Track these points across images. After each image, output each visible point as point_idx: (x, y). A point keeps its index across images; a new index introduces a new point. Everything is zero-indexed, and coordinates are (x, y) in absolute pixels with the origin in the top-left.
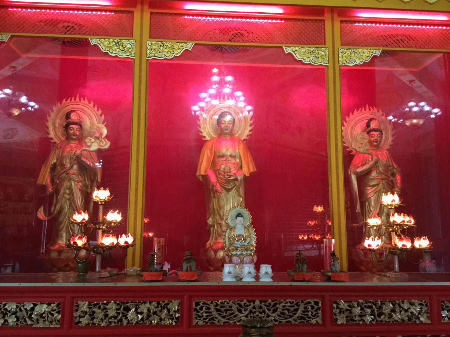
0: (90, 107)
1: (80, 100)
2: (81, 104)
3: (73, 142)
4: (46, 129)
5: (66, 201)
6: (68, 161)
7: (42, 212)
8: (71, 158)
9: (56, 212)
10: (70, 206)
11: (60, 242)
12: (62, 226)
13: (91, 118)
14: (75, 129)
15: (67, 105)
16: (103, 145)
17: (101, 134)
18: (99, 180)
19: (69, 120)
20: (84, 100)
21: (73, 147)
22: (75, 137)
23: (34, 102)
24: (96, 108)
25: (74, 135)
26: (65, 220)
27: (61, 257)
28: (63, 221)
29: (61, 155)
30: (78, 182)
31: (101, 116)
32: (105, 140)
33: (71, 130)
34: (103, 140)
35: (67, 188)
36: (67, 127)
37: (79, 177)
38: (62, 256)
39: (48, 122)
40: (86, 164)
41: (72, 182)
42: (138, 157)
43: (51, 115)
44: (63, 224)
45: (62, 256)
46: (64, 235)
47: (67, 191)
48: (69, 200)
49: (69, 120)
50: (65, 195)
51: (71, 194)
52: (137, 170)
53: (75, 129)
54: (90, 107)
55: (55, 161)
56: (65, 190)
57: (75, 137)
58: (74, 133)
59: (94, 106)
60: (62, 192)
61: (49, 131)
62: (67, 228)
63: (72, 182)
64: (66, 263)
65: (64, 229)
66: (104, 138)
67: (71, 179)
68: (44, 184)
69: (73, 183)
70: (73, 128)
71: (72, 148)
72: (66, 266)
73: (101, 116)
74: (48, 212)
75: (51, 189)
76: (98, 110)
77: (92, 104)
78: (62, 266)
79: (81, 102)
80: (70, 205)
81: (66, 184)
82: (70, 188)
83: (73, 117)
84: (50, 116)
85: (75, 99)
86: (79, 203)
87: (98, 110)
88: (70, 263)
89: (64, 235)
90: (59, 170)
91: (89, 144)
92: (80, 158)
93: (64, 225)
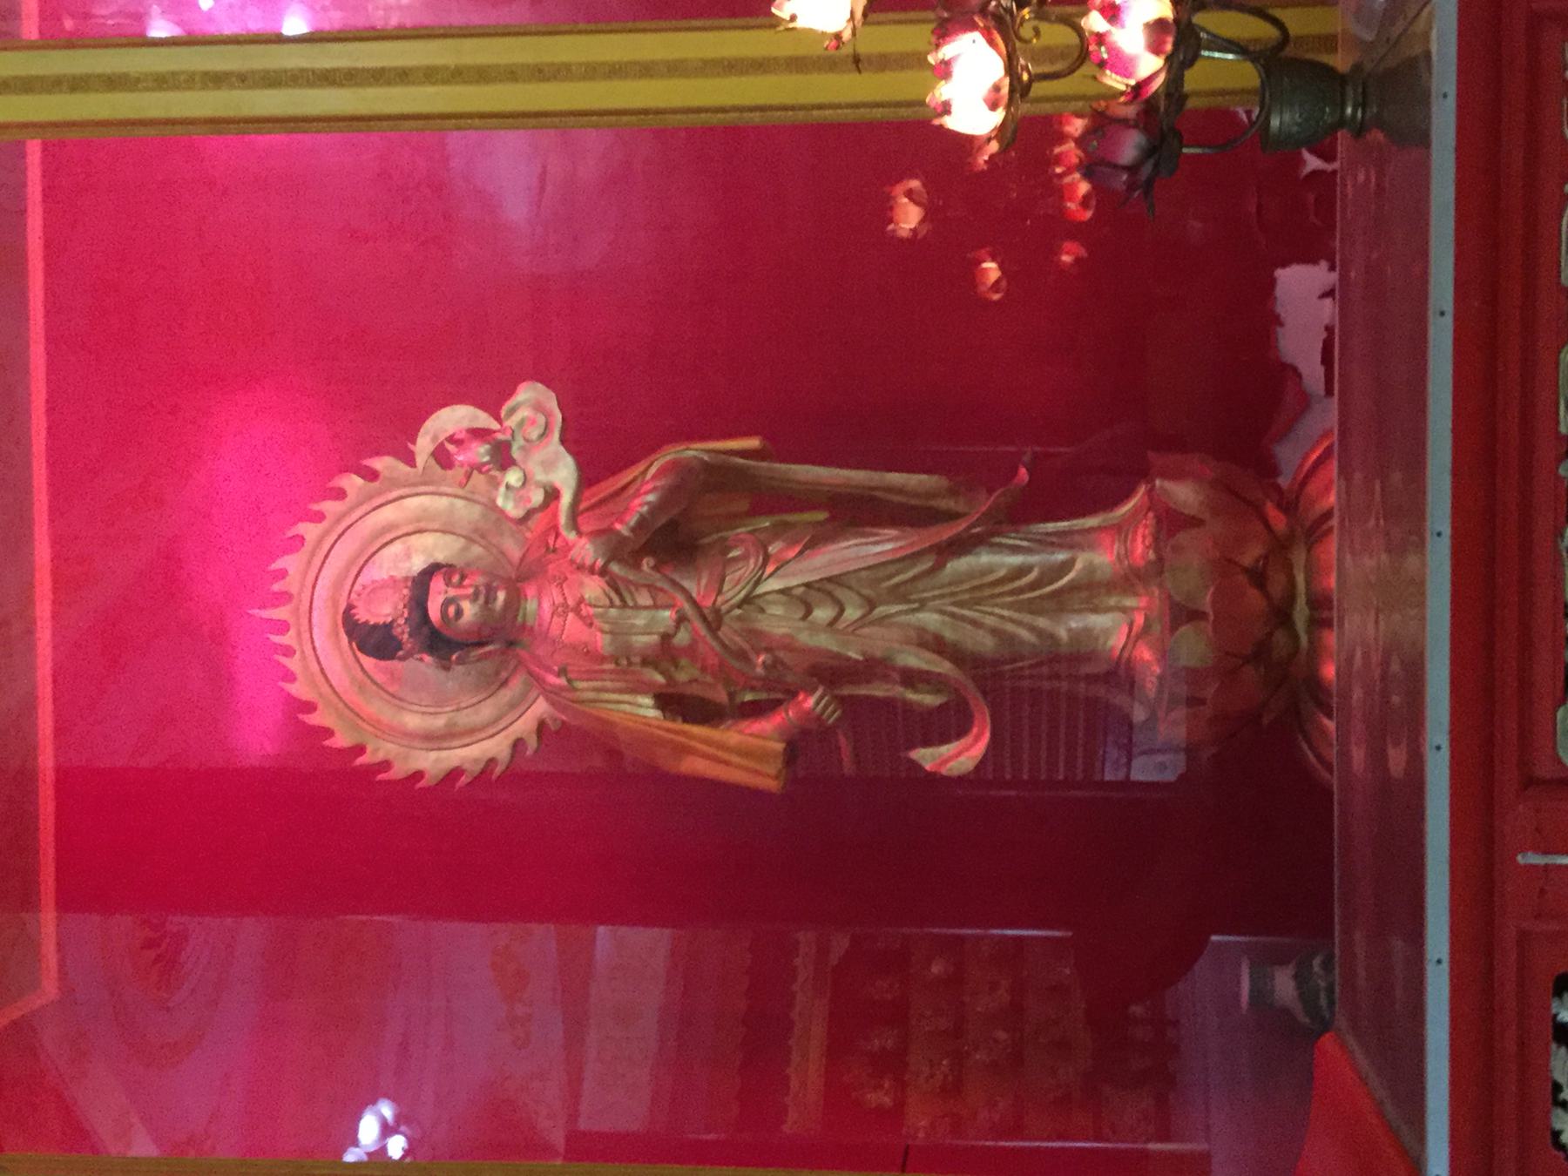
0: (320, 541)
1: (283, 598)
2: (326, 689)
3: (531, 606)
4: (464, 780)
5: (882, 621)
6: (640, 620)
7: (945, 750)
8: (624, 605)
9: (944, 667)
10: (904, 599)
11: (1117, 641)
12: (1025, 634)
13: (390, 527)
14: (452, 592)
15: (315, 668)
16: (541, 419)
17: (479, 434)
18: (753, 443)
19: (403, 632)
20: (282, 574)
21: (559, 600)
22: (501, 596)
23: (358, 1118)
24: (330, 507)
25: (490, 598)
26: (990, 621)
27: (1208, 609)
28: (994, 632)
29: (609, 666)
30: (767, 558)
31: (372, 475)
32: (513, 411)
33: (459, 613)
34: (512, 422)
35: (805, 618)
36: (440, 643)
37: (735, 559)
38: (1206, 602)
39: (418, 775)
40: (655, 509)
41: (761, 590)
42: (593, 72)
43: (380, 756)
44: (1010, 627)
45: (1206, 602)
46: (1075, 623)
47: (822, 614)
48: (871, 604)
49: (403, 632)
50: (841, 625)
51: (840, 593)
52: (675, 69)
53: (452, 592)
54: (320, 541)
55: (647, 701)
56: (814, 628)
57: (501, 596)
58: (474, 598)
59: (319, 517)
60: (825, 641)
61: (476, 761)
62: (1033, 607)
63: (761, 590)
64: (1242, 579)
65: (1042, 622)
66: (498, 419)
67: (747, 600)
68: (780, 747)
69: (773, 584)
70: (447, 603)
71: (565, 605)
72: (1258, 578)
73: (372, 475)
74: (947, 724)
75: (811, 701)
76: (340, 494)
77: (310, 531)
78: (1253, 596)
79: (294, 590)
80: (899, 594)
81: (778, 621)
82: (803, 600)
83: (385, 610)
84: (386, 765)
85: (283, 627)
86: (889, 546)
87: (340, 494)
88: (1247, 560)
89: (1075, 623)
90: (696, 673)
91: (537, 497)
92: (623, 540)
93: (1012, 620)
